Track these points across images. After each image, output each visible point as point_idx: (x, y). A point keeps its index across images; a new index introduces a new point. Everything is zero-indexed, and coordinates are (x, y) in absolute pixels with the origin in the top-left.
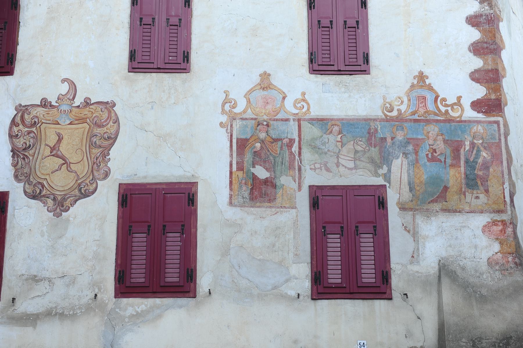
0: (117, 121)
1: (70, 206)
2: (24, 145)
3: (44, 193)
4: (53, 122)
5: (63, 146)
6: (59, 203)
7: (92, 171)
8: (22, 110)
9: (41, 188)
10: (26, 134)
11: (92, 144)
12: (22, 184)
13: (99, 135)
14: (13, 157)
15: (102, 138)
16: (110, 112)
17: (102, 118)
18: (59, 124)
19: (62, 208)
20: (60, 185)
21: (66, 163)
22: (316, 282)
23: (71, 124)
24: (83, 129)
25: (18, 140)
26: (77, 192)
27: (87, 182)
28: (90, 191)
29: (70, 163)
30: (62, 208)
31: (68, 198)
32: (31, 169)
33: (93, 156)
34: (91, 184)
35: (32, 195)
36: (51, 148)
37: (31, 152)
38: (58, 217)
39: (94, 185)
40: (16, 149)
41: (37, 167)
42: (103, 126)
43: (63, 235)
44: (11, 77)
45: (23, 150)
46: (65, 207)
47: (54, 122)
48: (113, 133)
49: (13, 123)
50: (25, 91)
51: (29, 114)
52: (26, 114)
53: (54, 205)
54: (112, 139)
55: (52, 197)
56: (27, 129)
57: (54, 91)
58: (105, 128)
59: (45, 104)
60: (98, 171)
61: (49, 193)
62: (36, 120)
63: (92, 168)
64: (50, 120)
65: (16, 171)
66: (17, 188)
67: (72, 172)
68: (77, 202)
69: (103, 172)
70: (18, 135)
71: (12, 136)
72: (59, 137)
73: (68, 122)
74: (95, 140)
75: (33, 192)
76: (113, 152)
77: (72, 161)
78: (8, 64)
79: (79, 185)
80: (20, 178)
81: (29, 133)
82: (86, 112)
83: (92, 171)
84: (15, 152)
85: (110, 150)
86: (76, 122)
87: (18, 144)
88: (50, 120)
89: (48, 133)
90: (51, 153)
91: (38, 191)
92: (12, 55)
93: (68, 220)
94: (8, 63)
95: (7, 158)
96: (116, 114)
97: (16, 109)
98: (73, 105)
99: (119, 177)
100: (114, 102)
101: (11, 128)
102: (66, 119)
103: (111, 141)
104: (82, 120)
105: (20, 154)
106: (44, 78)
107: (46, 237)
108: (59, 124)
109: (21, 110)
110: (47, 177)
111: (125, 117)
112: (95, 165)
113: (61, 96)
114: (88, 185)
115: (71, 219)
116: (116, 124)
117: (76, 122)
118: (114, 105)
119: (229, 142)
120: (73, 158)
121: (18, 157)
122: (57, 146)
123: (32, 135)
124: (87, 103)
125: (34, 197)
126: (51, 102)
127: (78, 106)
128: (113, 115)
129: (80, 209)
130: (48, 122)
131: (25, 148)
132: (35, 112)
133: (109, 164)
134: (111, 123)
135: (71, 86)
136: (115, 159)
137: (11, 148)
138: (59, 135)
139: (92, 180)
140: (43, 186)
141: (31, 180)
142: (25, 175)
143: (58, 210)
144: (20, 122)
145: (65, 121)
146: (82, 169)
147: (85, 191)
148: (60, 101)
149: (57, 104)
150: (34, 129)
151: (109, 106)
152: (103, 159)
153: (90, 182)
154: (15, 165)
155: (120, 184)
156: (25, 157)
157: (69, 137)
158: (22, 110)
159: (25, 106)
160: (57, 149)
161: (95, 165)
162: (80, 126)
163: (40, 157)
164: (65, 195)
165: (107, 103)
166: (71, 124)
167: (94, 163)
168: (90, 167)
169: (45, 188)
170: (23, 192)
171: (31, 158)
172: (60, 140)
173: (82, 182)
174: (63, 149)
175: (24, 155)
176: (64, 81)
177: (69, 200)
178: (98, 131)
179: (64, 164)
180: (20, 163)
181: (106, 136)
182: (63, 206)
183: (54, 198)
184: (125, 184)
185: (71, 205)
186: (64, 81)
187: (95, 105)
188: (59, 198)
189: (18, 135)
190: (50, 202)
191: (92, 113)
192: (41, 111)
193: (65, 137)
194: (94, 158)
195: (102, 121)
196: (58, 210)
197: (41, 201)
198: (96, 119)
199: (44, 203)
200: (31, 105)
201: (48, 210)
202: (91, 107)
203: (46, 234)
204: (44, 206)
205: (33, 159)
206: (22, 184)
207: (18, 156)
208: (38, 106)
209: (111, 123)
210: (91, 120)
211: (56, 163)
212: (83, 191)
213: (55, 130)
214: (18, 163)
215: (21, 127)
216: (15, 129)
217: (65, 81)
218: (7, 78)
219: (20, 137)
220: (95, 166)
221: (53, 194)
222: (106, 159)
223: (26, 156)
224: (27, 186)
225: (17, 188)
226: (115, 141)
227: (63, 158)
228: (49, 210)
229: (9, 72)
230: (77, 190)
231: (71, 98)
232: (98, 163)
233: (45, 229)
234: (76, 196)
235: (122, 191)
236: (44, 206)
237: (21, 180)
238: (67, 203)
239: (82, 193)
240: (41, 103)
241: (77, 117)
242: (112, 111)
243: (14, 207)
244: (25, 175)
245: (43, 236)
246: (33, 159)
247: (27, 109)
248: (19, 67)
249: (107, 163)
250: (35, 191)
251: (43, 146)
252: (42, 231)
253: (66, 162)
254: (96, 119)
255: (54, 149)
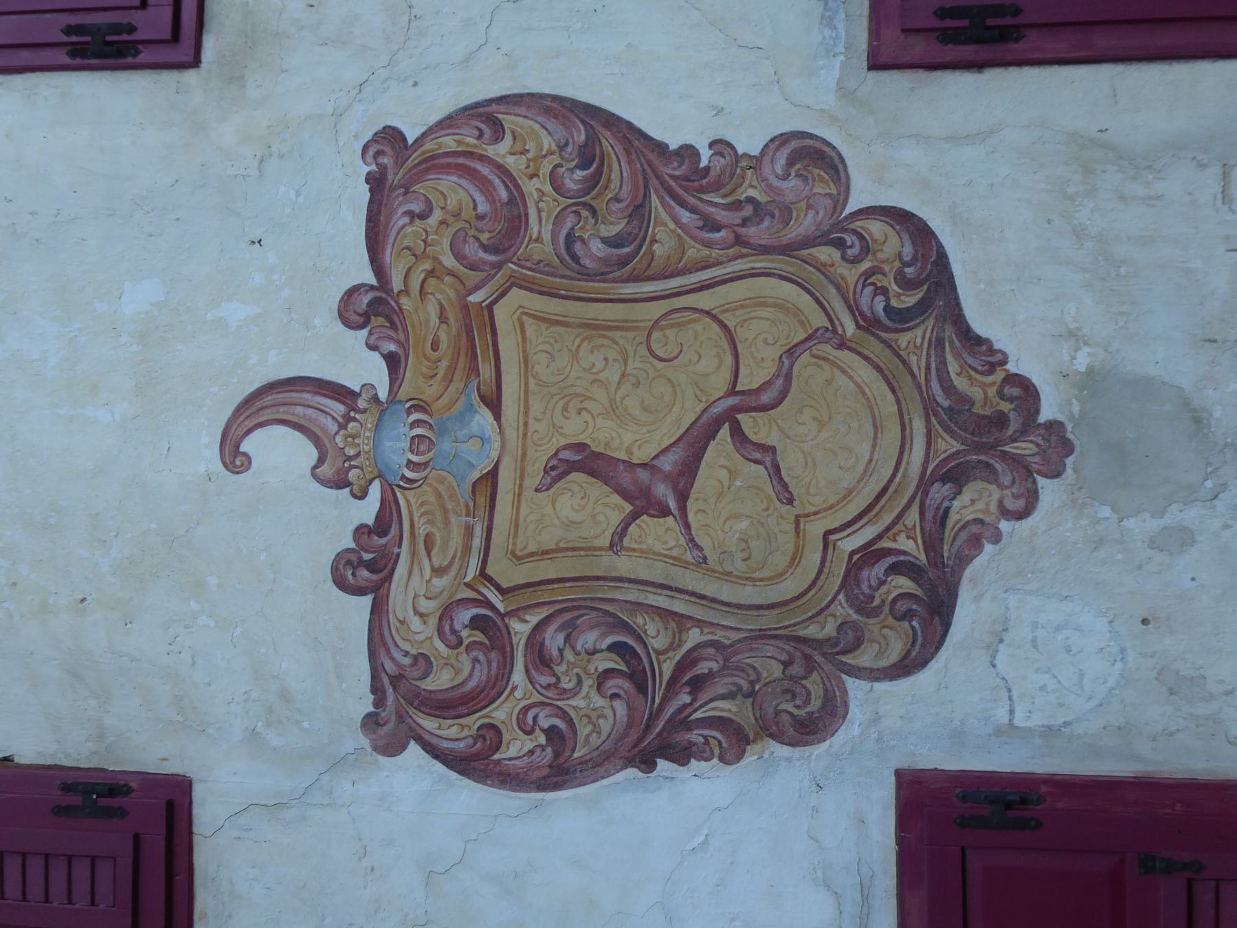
0: (486, 116)
1: (999, 376)
2: (613, 684)
3: (910, 546)
4: (482, 512)
5: (628, 438)
6: (978, 448)
7: (787, 250)
8: (402, 709)
9: (879, 569)
10: (545, 680)
11: (623, 262)
12: (856, 688)
13: (570, 221)
14: (682, 755)
15: (584, 203)
16: (435, 164)
17: (468, 213)
18: (492, 476)
19: (1014, 424)
20: (866, 447)
21: (729, 416)
22: (1004, 35)
23: (494, 403)
24: (531, 327)
25: (584, 730)
26: (914, 339)
27: (850, 274)
28: (908, 251)
29: (732, 392)
30: (1014, 424)
31: (948, 387)
32: (763, 635)
33: (694, 252)
34: (866, 250)
35: (926, 625)
36: (634, 516)
37: (656, 636)
38: (1067, 447)
39: (876, 228)
40: (634, 736)
41: (748, 595)
42: (517, 199)
43: (1186, 404)
44: (198, 792)
45: (642, 688)
46: (1005, 406)
47: (482, 501)
48: (560, 133)
49: (477, 763)
50: (285, 696)
51: (423, 662)
52: (429, 684)
53: (990, 474)
54: (595, 133)
55: (939, 491)
56: (518, 676)
57: (297, 510)
58: (530, 188)
59: (365, 568)
60: (786, 213)
61: (913, 516)
62: (465, 616)
63: (765, 250)
64: (469, 532)
65: (771, 730)
66: (876, 719)
67: (788, 378)
68: (979, 324)
69: (793, 183)
70: (551, 732)
71: (559, 770)
72: (571, 467)
73: (484, 417)
74: (597, 247)
75: (908, 615)
76: (675, 121)
77: (719, 383)
78: (121, 813)
79: (868, 324)
80: (815, 704)
81: (540, 659)
82: (426, 315)
83: (787, 250)
84: (654, 745)
85: (660, 148)
86: (486, 371)
87: (606, 727)
88: (469, 532)
89: (548, 539)
90: (664, 512)
91: (904, 584)
92: (68, 788)
93: (1091, 383)
94: (110, 813)
95: (693, 793)
96: (448, 123)
97: (392, 748)
98: (383, 394)
99: (830, 75)
100: (376, 138)
101: (508, 779)
102: (461, 434)
103: (609, 143)
104: (476, 328)
105: (670, 710)
106: (213, 581)
107: (1191, 515)
108: (492, 476)
109: (401, 718)
110: (815, 529)
111: (467, 60)
112: (751, 232)
113: (326, 470)
114: (868, 274)
115: (1082, 362)
116: (508, 121)
117: (486, 371)
118: (390, 137)
119: (717, 289)
120: (701, 373)
121: (687, 725)
122: (625, 480)
123: (553, 640)
124: (370, 310)
125: (934, 611)
126: (361, 531)
127: (393, 362)
128: (449, 142)
129: (1024, 314)
130: (477, 542)
131: (631, 677)
132: (415, 623)
133: (749, 143)
134: (500, 151)
135: (282, 413)
136: (719, 111)
137: (632, 772)
138: (558, 470)
139: (840, 244)
140: (869, 554)
141: (830, 629)
142: (797, 669)
143: (1024, 448)
144: (474, 722)
145: (477, 439)
146: (768, 311)
147: (907, 284)
148: (353, 475)
149: (375, 490)
150: (520, 629)
151: (395, 167)
152: (716, 187)
153: (855, 261)
154: (735, 742)
155: (877, 63)
156: (689, 677)
157: (574, 405)
158: (402, 709)
159: (377, 689)
160: (643, 475)
161: (751, 232)
162: (508, 345)
163: (689, 580)
164: (930, 408)
165: (376, 182)
166: (494, 403)
167: (739, 240)
168: (761, 263)
169: (886, 544)
170: (903, 684)
171: (694, 637)
172: (587, 461)
173: (854, 308)
174: (642, 438)
175: (672, 682)
176: (233, 456)
177: (960, 383)
178: (540, 226)
179: (737, 432)
180: (725, 708)
181: (574, 179)
182: (1000, 421)
183: (944, 479)
184: (875, 32)
185: (992, 368)
186: (233, 456)
187: (388, 257)
188: (947, 445)
189: (551, 732)
190: (972, 502)
191: (431, 273)
192: (413, 590)
193: (575, 429)
194: (708, 244)
195: (483, 207)
196: (1024, 448)
197: (963, 561)
198: (472, 250)
199: (976, 543)
200: (372, 654)
201: (1021, 515)
202: (397, 283)
203: (1177, 515)
204: (997, 538)
205: (700, 623)
206: (856, 688)
207: (681, 722)
208: (378, 610)
209: (500, 151)
210: (474, 277)
211: (733, 475)
212: (910, 300)
213: (529, 493)
214: (720, 723)
215: (501, 713)
216: (515, 748)
217: (236, 451)
218: (208, 813)
219: (563, 714)
220: (758, 233)
221: (924, 485)
222: (719, 163)
223: (680, 668)
224: (865, 658)
225: (876, 719)
226: (611, 121)
227: (696, 441)
228: (1020, 504)
229: (170, 806)
230: (903, 340)
231: (338, 408)
232: (735, 218)
233: (1141, 526)
234: (939, 343)
235: (919, 47)
236: (997, 538)
237: (828, 697)
238: (979, 391)
239: (922, 308)
240: (358, 591)
241: (452, 368)
242: (429, 146)
243: (999, 732)
244: (797, 669)
245: (1185, 538)
246: (700, 623)
247: (396, 680)
248: (146, 751)
249: (737, 158)
250: (901, 607)
251: (624, 565)
252: (1153, 544)
253: (725, 420)
254: (472, 250)
255: (646, 492)
